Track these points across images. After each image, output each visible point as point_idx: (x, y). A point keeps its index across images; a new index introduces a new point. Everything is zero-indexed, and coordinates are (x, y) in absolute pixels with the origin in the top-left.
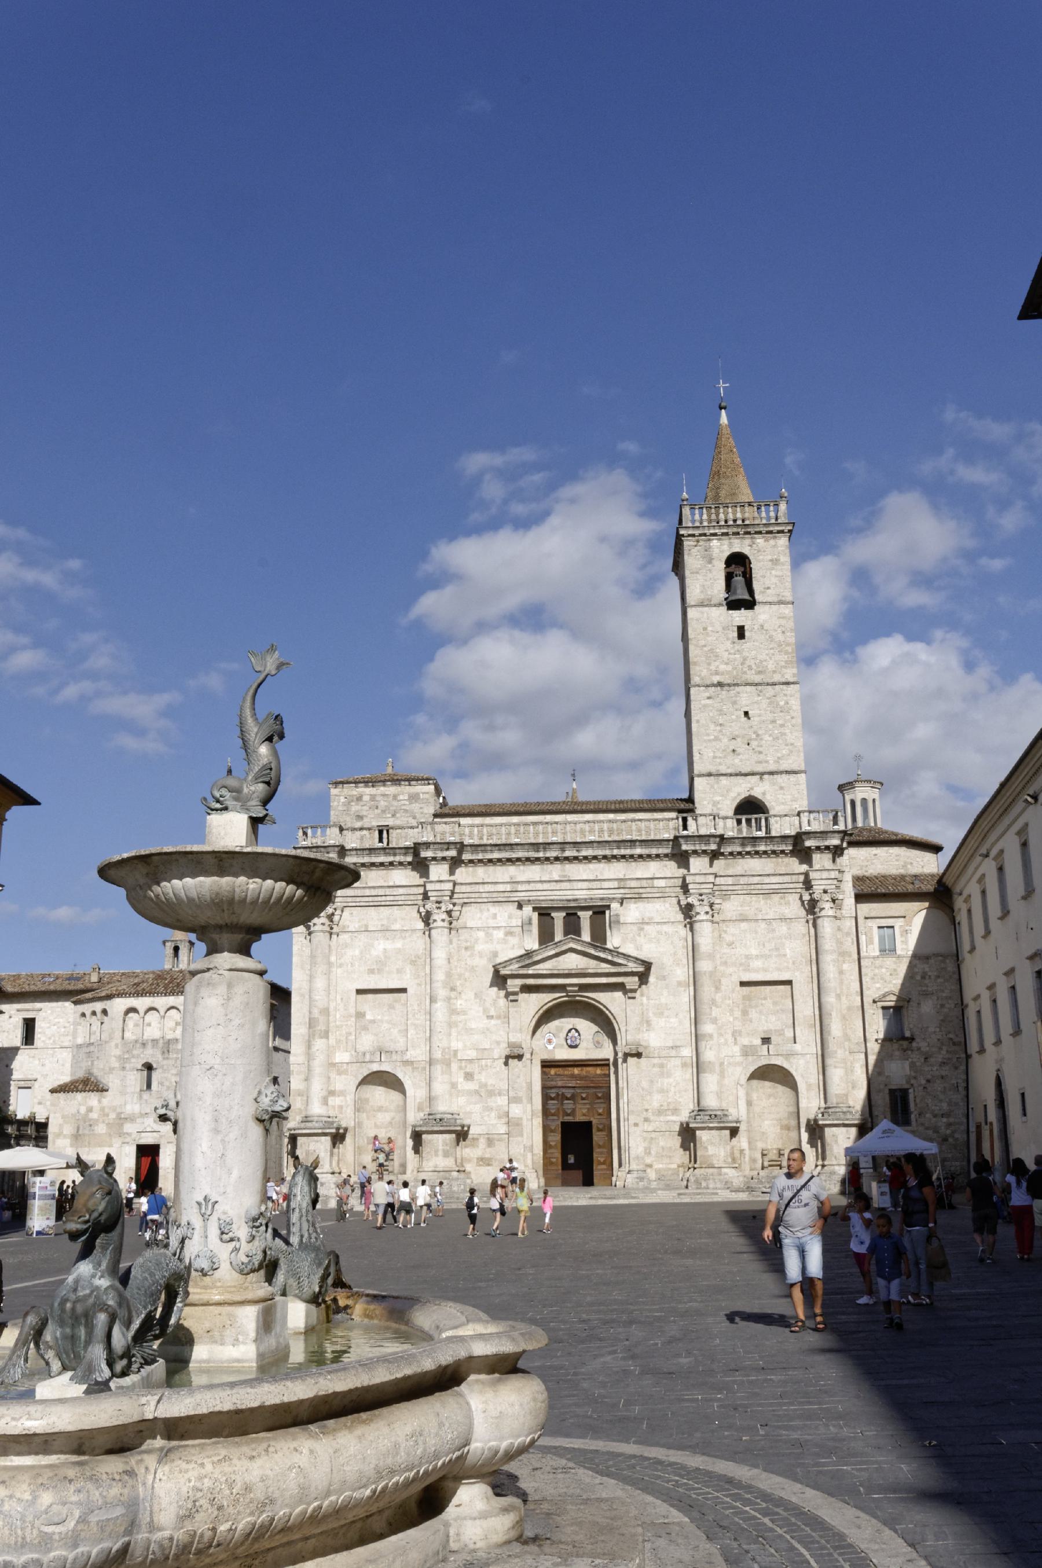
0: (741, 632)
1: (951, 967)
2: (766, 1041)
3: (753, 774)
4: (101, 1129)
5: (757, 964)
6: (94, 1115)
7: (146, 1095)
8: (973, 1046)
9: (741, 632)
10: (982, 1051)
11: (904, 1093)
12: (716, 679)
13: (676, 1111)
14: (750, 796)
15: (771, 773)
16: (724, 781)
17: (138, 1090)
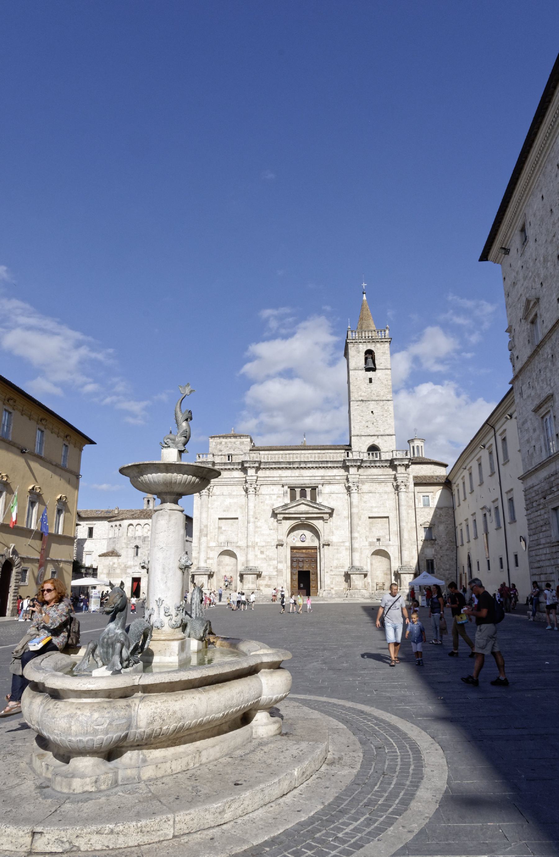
0: (371, 380)
1: (451, 511)
2: (378, 540)
4: (118, 571)
6: (115, 566)
7: (136, 558)
8: (459, 543)
9: (371, 380)
10: (462, 545)
13: (343, 567)
15: (382, 435)
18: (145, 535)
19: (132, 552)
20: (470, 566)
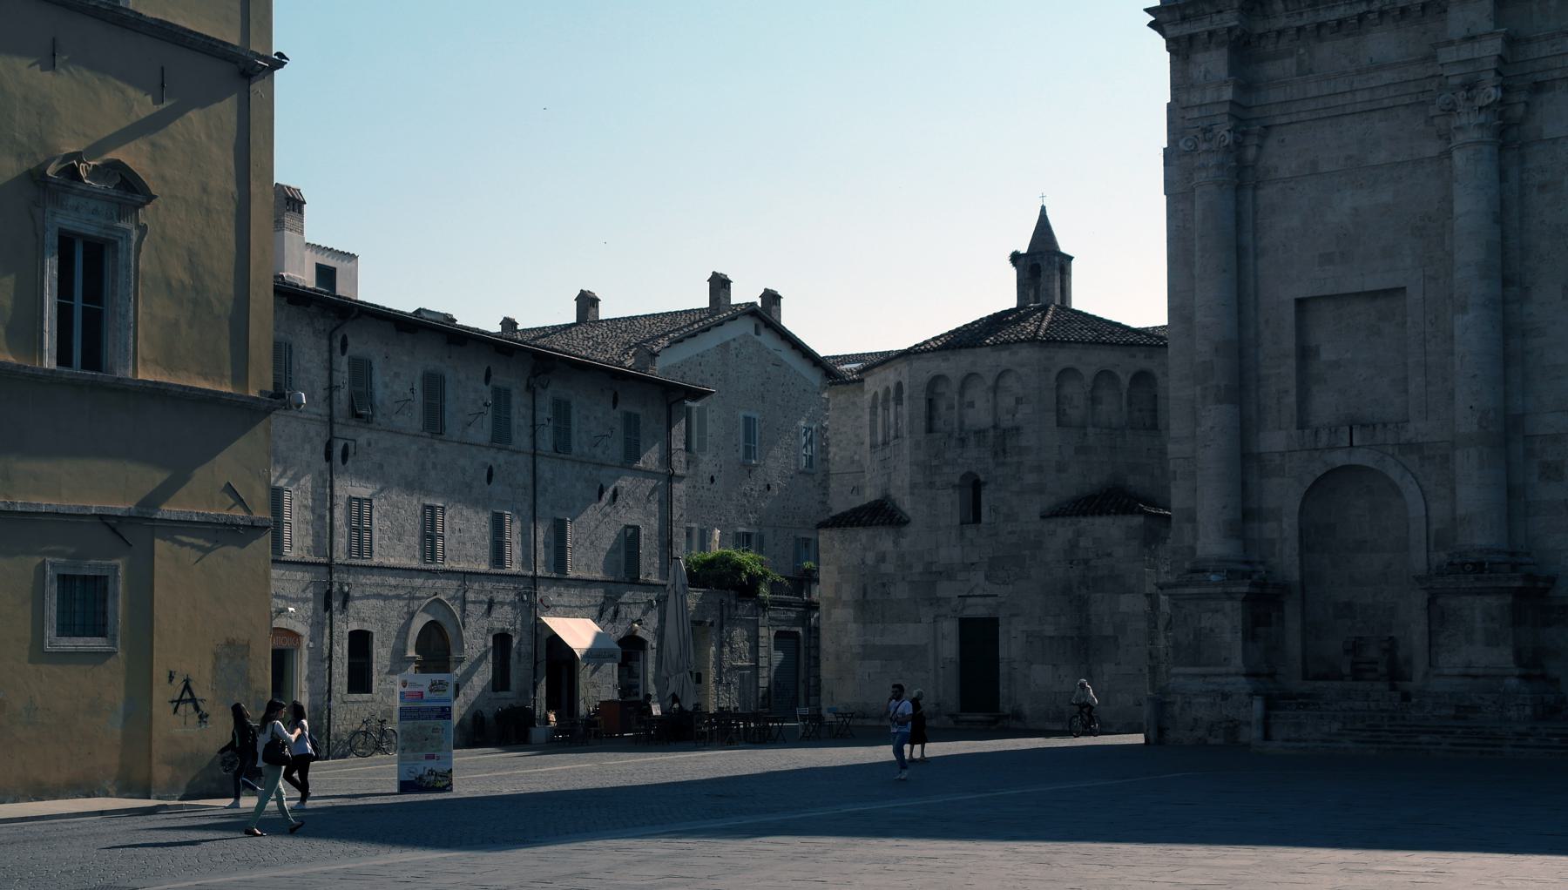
4: (900, 592)
6: (888, 568)
7: (970, 532)
14: (243, 546)
17: (957, 521)
18: (1007, 421)
19: (950, 504)
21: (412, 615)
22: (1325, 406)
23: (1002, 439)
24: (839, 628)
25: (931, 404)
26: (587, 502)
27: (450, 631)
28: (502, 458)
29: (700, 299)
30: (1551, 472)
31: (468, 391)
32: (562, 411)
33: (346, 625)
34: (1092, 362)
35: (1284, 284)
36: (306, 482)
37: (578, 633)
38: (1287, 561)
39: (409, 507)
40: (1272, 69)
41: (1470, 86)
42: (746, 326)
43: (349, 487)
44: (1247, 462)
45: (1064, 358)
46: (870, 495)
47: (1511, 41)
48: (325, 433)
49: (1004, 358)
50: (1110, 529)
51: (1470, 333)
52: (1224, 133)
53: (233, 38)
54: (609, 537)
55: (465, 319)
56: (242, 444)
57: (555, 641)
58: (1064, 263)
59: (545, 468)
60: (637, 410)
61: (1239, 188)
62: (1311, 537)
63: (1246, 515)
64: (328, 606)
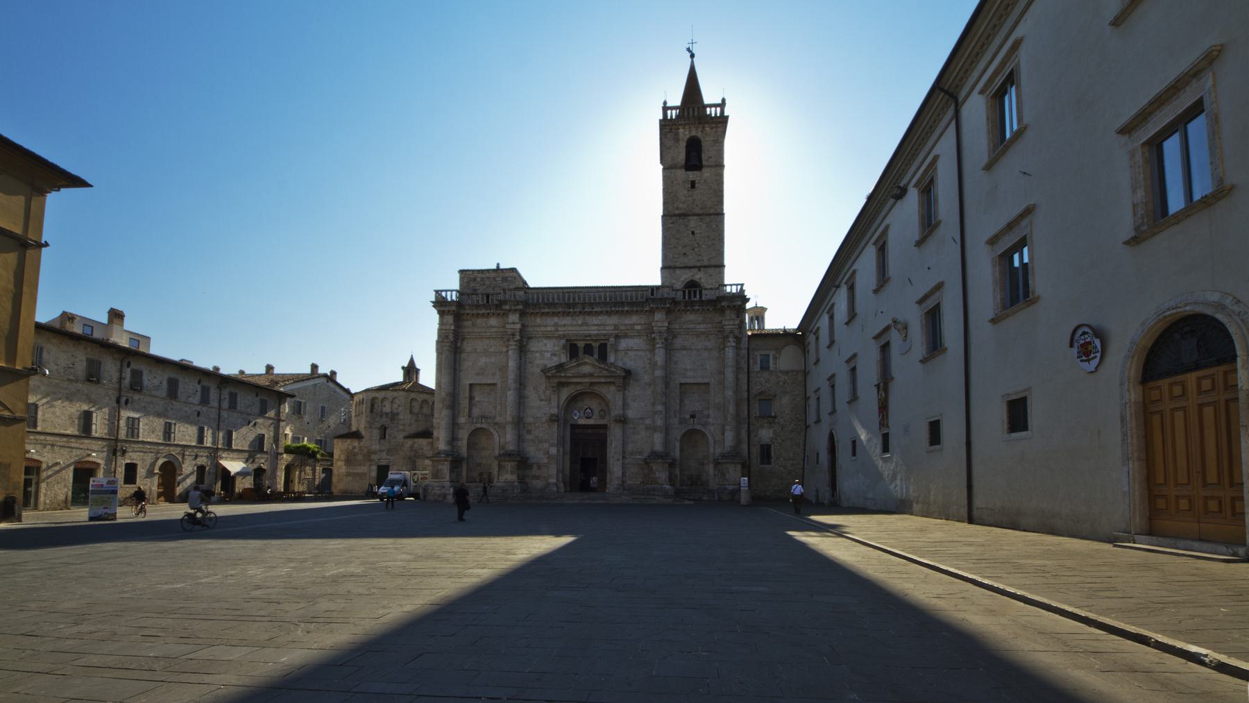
0: (693, 184)
1: (800, 377)
2: (693, 416)
3: (694, 267)
4: (360, 457)
5: (690, 374)
8: (812, 418)
9: (693, 184)
10: (818, 421)
11: (769, 447)
12: (677, 212)
13: (640, 453)
15: (705, 267)
16: (678, 271)
20: (832, 450)
21: (157, 459)
22: (476, 412)
23: (393, 416)
24: (339, 467)
25: (372, 405)
26: (242, 426)
27: (176, 464)
28: (204, 409)
29: (308, 371)
30: (529, 432)
31: (189, 387)
32: (233, 398)
33: (122, 462)
34: (421, 397)
35: (467, 380)
36: (106, 410)
37: (234, 466)
38: (464, 451)
39: (159, 423)
40: (466, 323)
41: (513, 335)
42: (324, 380)
43: (126, 414)
44: (454, 425)
45: (413, 395)
46: (354, 429)
47: (523, 326)
48: (116, 394)
49: (395, 394)
50: (423, 442)
51: (511, 396)
52: (451, 337)
53: (18, 230)
54: (251, 437)
55: (224, 371)
56: (10, 387)
57: (225, 471)
58: (417, 371)
59: (224, 414)
60: (233, 390)
61: (455, 353)
62: (471, 445)
63: (453, 439)
64: (115, 453)
